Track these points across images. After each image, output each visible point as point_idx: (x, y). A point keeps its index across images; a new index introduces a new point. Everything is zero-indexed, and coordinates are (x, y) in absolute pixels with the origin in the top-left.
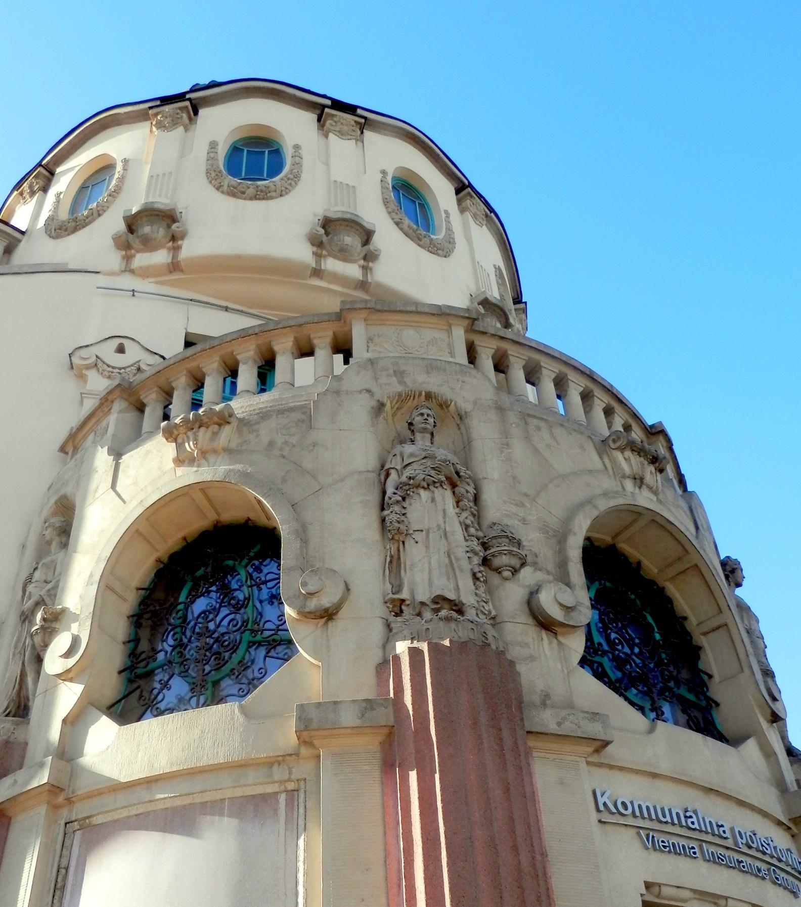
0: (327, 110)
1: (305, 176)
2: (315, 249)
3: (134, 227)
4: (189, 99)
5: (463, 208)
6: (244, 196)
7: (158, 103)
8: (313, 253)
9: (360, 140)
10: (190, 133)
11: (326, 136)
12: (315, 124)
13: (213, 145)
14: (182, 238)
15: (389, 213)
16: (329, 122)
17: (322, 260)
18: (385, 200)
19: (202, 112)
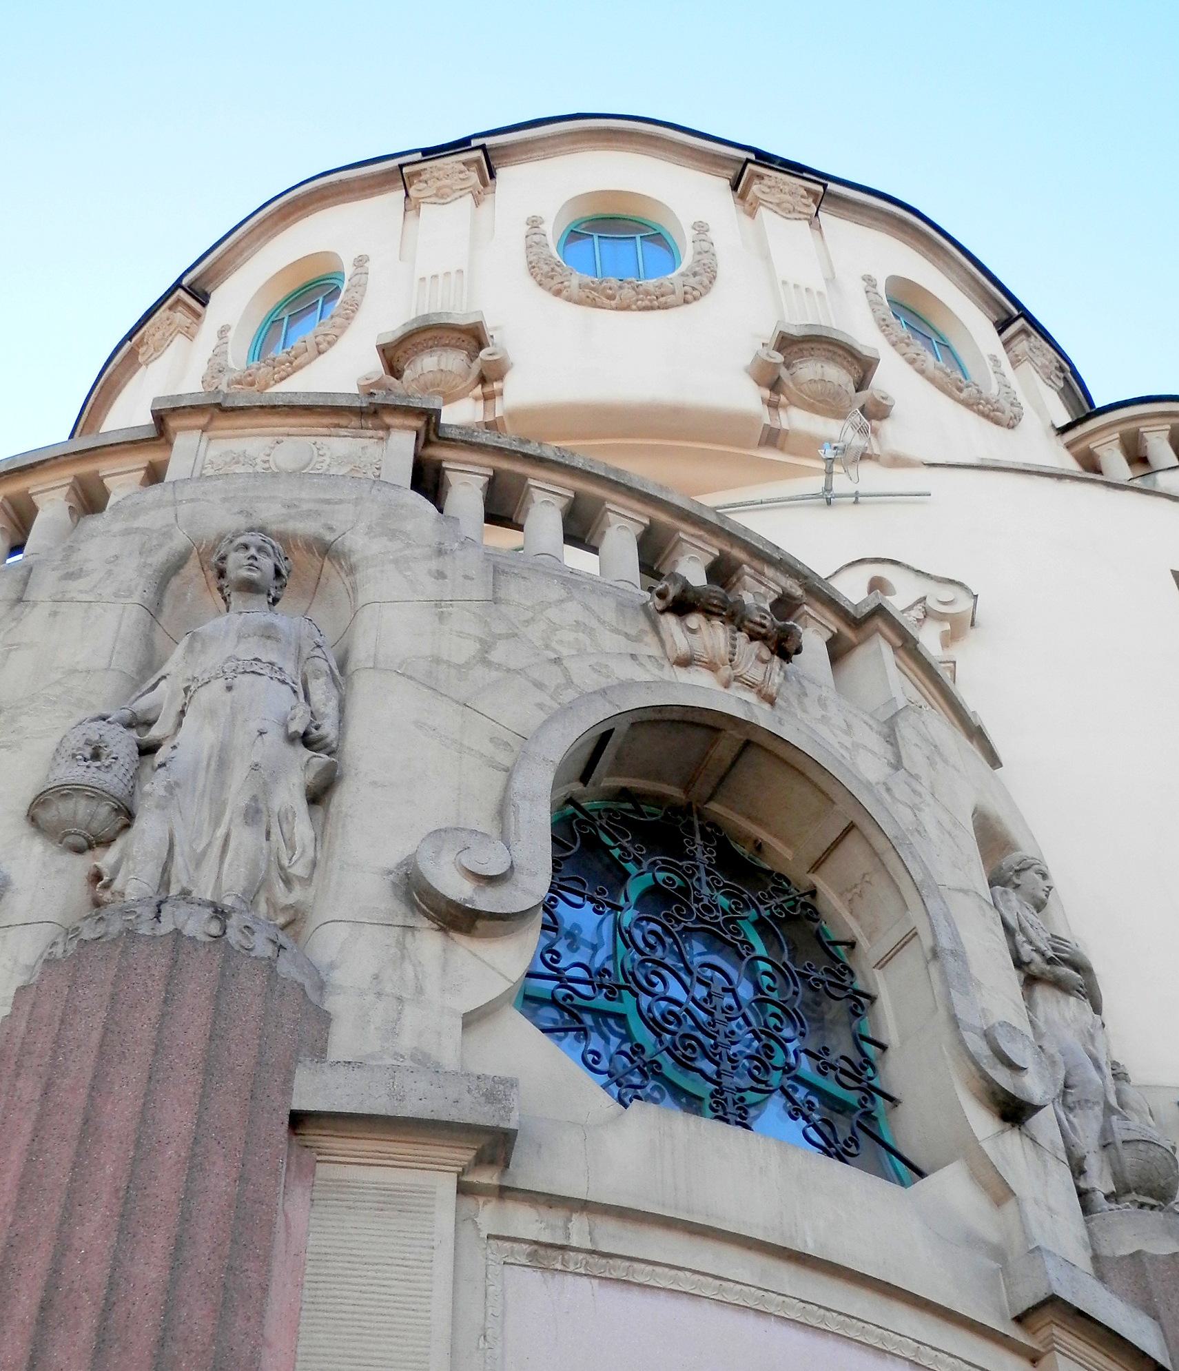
0: (750, 166)
1: (723, 271)
2: (767, 393)
3: (399, 366)
4: (482, 147)
5: (1017, 356)
6: (613, 303)
7: (418, 156)
8: (763, 400)
9: (813, 221)
10: (485, 207)
11: (752, 214)
12: (729, 196)
13: (534, 223)
14: (500, 378)
15: (894, 345)
16: (755, 188)
17: (782, 413)
18: (882, 323)
19: (501, 173)
